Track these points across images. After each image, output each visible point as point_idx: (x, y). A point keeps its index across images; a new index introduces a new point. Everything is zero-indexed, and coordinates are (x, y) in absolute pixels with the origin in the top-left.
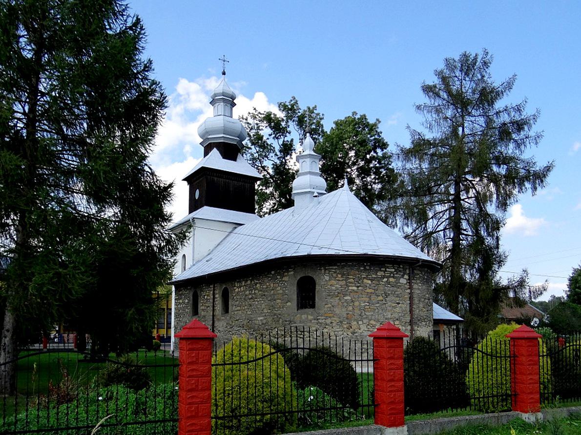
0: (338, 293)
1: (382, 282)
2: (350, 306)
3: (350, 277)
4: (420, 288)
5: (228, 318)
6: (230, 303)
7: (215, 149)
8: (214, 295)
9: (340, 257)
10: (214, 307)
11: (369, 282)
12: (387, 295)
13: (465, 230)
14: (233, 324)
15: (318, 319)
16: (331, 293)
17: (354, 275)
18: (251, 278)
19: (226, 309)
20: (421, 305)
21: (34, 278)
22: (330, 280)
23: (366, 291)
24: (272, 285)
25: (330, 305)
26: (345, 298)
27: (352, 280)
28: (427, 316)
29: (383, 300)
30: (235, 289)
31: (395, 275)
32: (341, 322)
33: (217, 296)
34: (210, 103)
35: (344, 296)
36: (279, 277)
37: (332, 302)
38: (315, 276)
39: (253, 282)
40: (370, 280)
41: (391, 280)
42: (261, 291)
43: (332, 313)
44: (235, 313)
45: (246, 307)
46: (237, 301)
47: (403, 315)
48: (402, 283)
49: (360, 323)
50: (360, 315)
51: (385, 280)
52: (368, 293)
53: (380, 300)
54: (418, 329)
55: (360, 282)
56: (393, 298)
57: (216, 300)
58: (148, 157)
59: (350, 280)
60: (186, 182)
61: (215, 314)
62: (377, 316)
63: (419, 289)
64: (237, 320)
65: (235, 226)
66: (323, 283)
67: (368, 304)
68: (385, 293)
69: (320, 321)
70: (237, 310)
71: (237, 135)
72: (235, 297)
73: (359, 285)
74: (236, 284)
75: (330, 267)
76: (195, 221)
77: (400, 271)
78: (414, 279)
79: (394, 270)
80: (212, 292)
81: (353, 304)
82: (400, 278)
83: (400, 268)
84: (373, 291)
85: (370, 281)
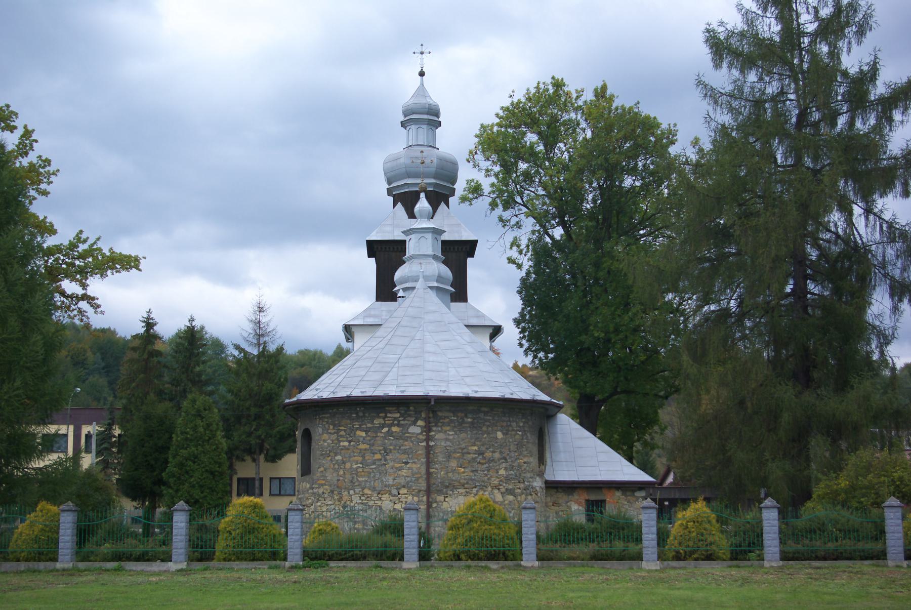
1: (381, 433)
11: (364, 434)
12: (387, 452)
26: (337, 458)
29: (381, 460)
31: (402, 422)
40: (364, 431)
41: (395, 429)
48: (413, 434)
51: (385, 430)
52: (361, 449)
56: (397, 455)
62: (372, 483)
67: (361, 466)
68: (385, 450)
77: (410, 416)
78: (436, 425)
79: (398, 415)
82: (410, 425)
83: (411, 411)
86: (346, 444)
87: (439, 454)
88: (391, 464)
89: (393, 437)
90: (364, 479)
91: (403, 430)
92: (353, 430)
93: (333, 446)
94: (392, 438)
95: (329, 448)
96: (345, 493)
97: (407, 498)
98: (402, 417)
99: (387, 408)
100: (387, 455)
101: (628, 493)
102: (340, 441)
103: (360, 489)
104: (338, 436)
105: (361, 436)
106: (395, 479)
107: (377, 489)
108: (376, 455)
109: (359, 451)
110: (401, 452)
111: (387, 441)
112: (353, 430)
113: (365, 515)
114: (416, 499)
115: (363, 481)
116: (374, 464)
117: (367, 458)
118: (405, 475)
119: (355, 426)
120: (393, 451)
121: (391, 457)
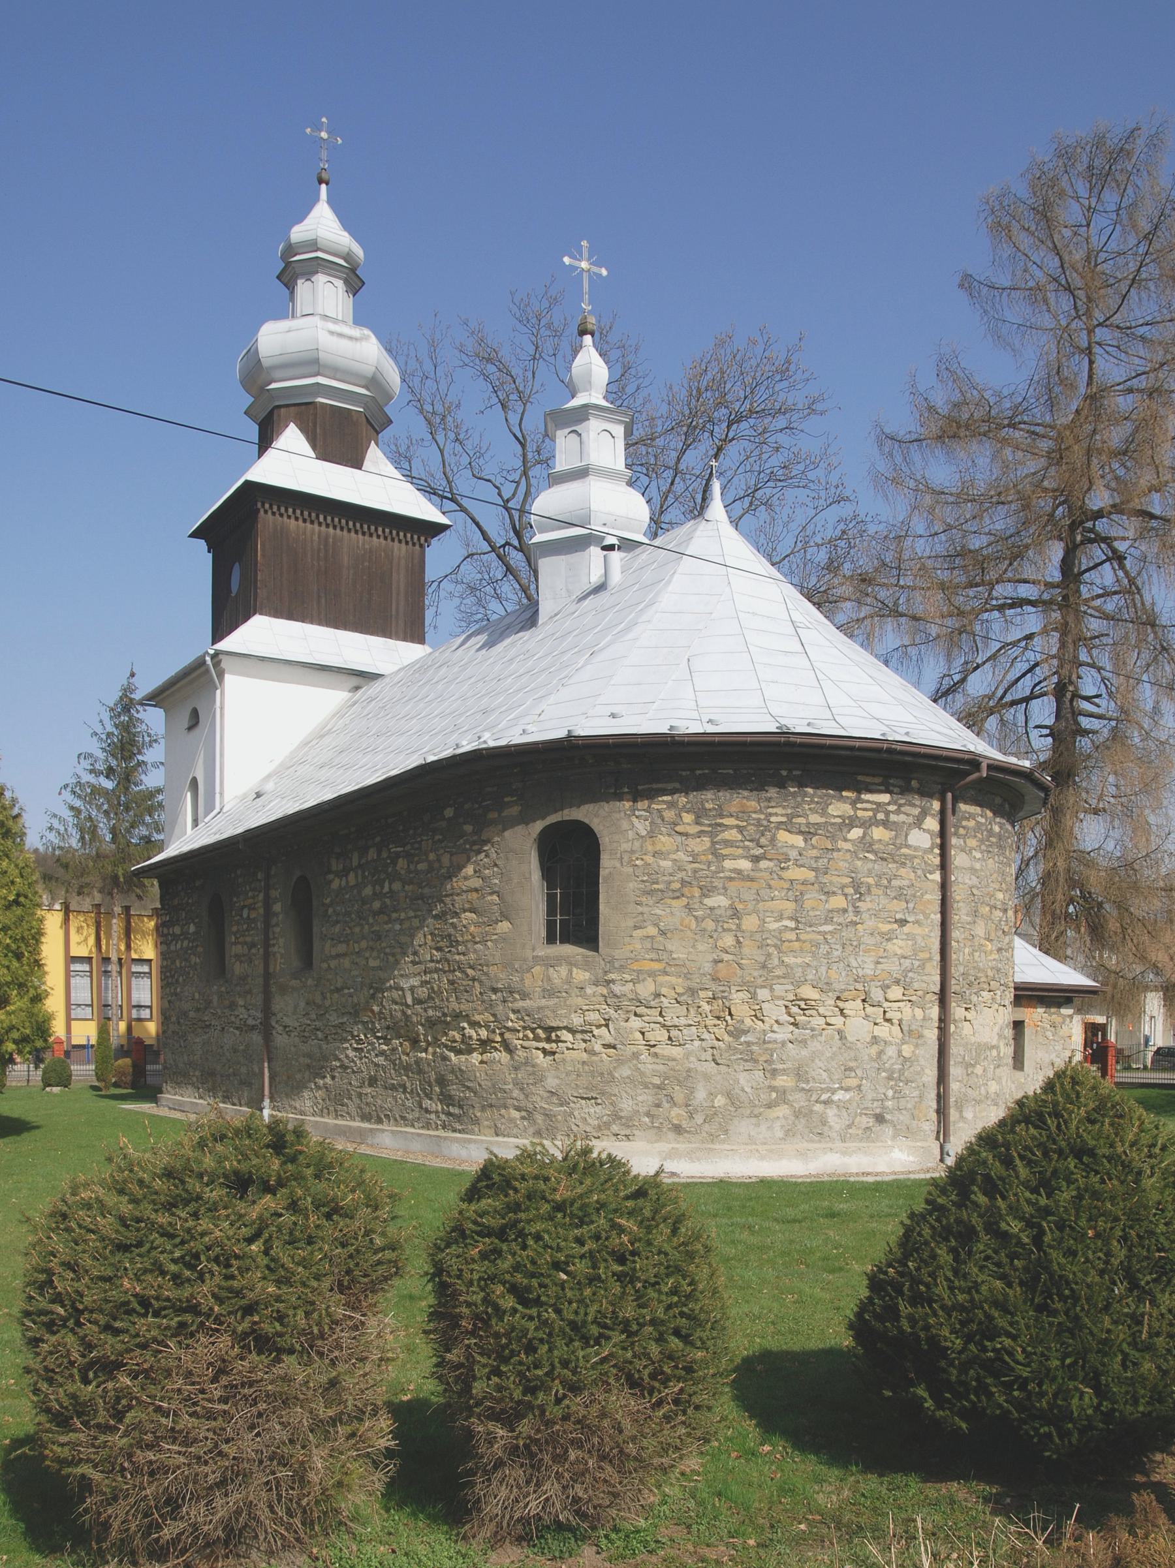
0: (683, 882)
1: (846, 840)
2: (724, 930)
3: (726, 821)
4: (978, 866)
5: (310, 982)
6: (315, 929)
7: (292, 425)
8: (267, 905)
9: (690, 744)
10: (267, 945)
11: (799, 841)
12: (860, 890)
13: (1087, 699)
14: (328, 1003)
15: (609, 982)
16: (657, 883)
17: (743, 814)
18: (378, 839)
19: (307, 960)
20: (980, 930)
21: (1148, 1183)
22: (651, 835)
23: (788, 875)
24: (446, 860)
25: (652, 931)
26: (709, 902)
27: (732, 835)
28: (998, 970)
29: (845, 911)
30: (331, 882)
31: (893, 818)
32: (692, 992)
33: (277, 907)
34: (278, 277)
35: (704, 895)
36: (468, 828)
37: (659, 917)
38: (596, 821)
39: (384, 855)
40: (801, 832)
41: (878, 833)
42: (411, 883)
43: (659, 960)
44: (333, 963)
45: (364, 944)
46: (337, 922)
47: (917, 963)
48: (916, 849)
49: (763, 994)
50: (764, 967)
51: (856, 833)
52: (791, 881)
53: (838, 911)
54: (969, 1016)
55: (763, 841)
56: (884, 901)
57: (274, 921)
58: (867, 1275)
59: (726, 835)
60: (201, 544)
61: (271, 970)
62: (823, 969)
63: (973, 870)
64: (338, 990)
65: (355, 681)
66: (626, 846)
67: (792, 924)
68: (856, 885)
69: (617, 989)
70: (338, 956)
71: (363, 383)
72: (330, 911)
73: (761, 851)
74: (333, 862)
75: (655, 786)
76: (223, 665)
80: (261, 897)
81: (739, 926)
82: (910, 826)
84: (811, 875)
85: (801, 838)
86: (745, 865)
87: (961, 904)
88: (870, 923)
89: (875, 853)
90: (799, 960)
91: (896, 836)
92: (764, 828)
93: (695, 871)
94: (871, 856)
95: (680, 875)
96: (738, 998)
97: (900, 1010)
98: (895, 803)
99: (860, 778)
100: (859, 899)
101: (1053, 1010)
102: (724, 857)
103: (791, 987)
104: (713, 843)
105: (793, 846)
106: (878, 963)
107: (836, 986)
108: (833, 899)
109: (787, 885)
110: (893, 895)
111: (859, 863)
112: (767, 828)
113: (804, 1052)
114: (919, 1012)
115: (798, 966)
116: (828, 920)
117: (808, 905)
118: (899, 952)
119: (773, 819)
120: (874, 890)
121: (869, 905)
